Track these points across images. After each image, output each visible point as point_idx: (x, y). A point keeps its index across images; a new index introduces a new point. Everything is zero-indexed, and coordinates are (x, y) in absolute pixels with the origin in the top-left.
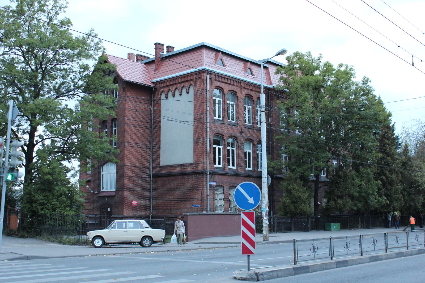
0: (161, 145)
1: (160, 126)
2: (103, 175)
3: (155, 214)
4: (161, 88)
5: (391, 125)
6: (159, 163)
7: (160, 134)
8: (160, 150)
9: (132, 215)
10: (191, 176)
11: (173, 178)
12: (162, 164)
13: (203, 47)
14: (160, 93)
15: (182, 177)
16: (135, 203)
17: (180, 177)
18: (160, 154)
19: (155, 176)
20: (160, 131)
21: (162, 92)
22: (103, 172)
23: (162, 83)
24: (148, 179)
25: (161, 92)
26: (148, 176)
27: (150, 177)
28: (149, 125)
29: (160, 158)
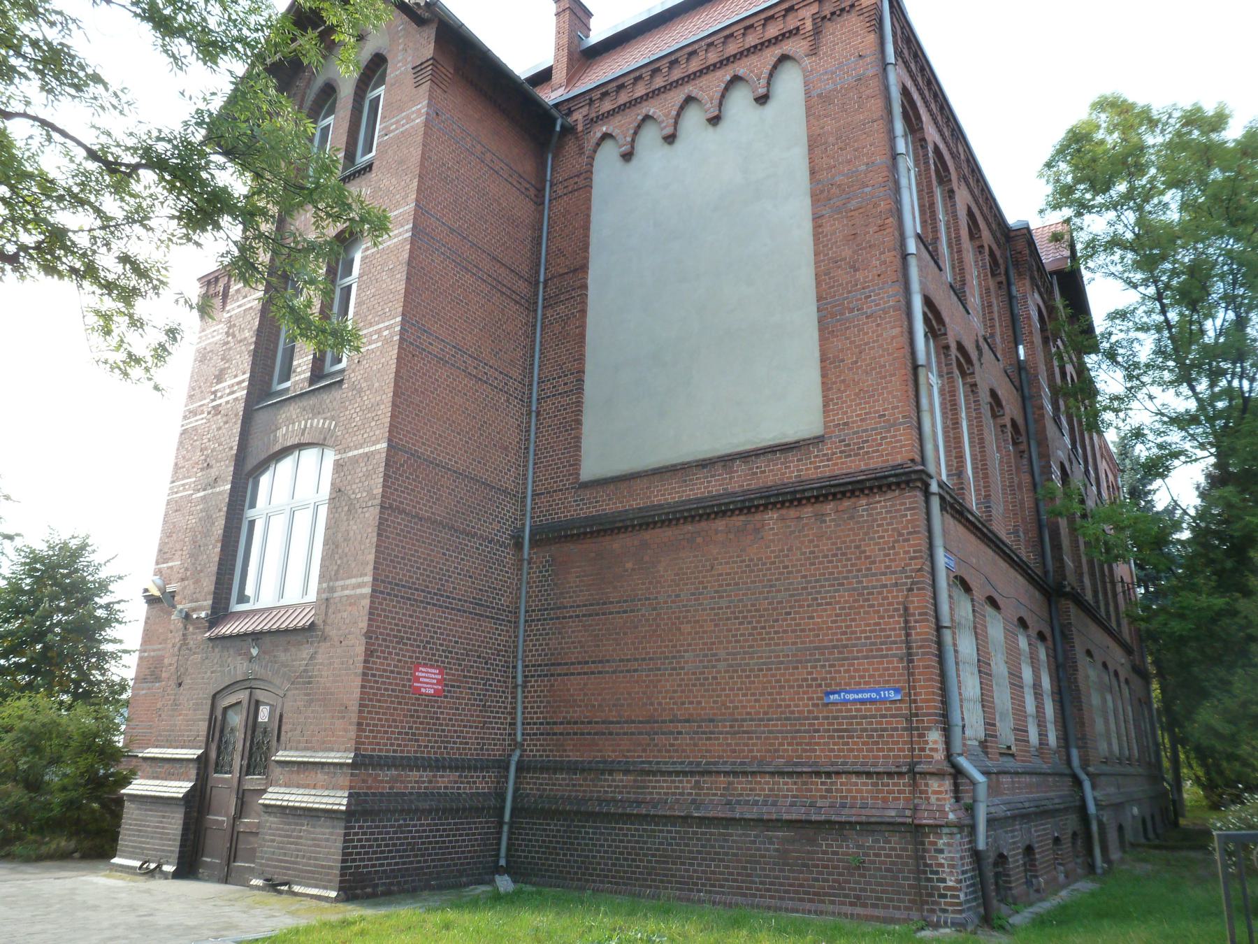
0: (588, 379)
1: (585, 287)
2: (252, 524)
3: (535, 751)
4: (592, 122)
5: (1149, 487)
6: (576, 464)
7: (583, 326)
8: (579, 403)
9: (410, 750)
10: (808, 511)
11: (667, 534)
12: (591, 468)
13: (214, 696)
14: (589, 146)
15: (738, 520)
16: (428, 679)
17: (720, 524)
18: (579, 422)
19: (554, 535)
20: (583, 312)
21: (606, 136)
22: (253, 505)
23: (605, 94)
24: (509, 556)
25: (599, 135)
26: (505, 538)
27: (518, 545)
28: (522, 286)
29: (578, 439)
